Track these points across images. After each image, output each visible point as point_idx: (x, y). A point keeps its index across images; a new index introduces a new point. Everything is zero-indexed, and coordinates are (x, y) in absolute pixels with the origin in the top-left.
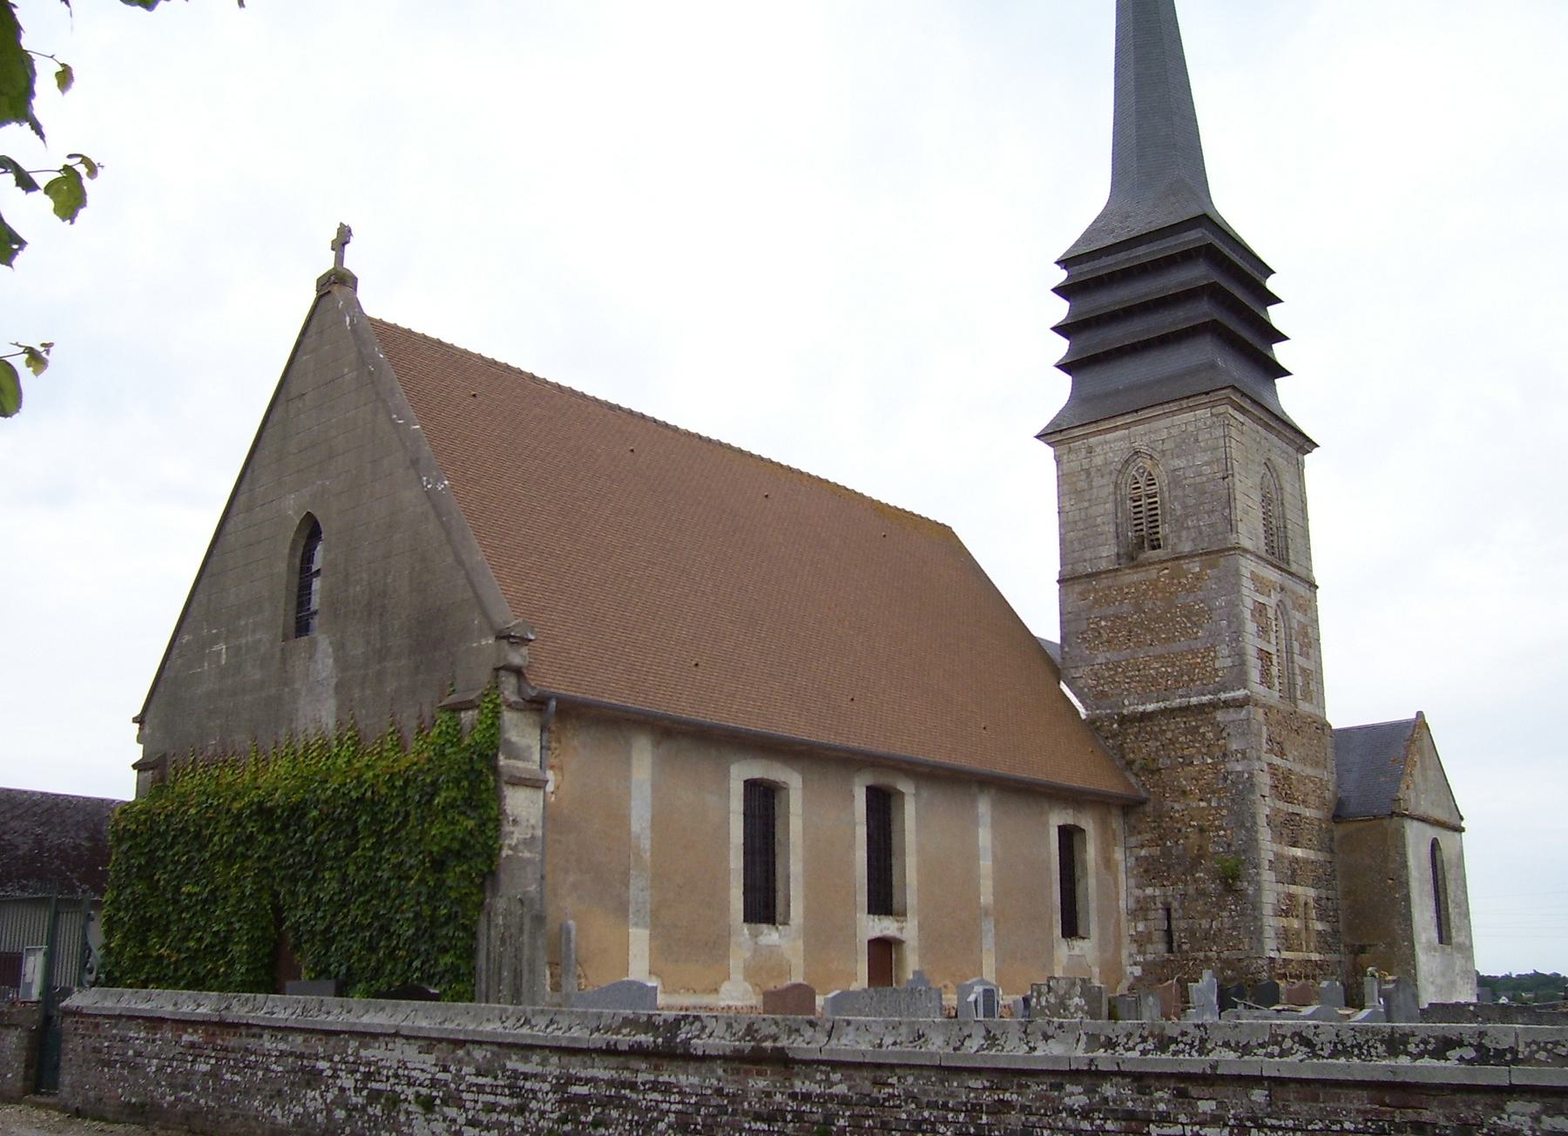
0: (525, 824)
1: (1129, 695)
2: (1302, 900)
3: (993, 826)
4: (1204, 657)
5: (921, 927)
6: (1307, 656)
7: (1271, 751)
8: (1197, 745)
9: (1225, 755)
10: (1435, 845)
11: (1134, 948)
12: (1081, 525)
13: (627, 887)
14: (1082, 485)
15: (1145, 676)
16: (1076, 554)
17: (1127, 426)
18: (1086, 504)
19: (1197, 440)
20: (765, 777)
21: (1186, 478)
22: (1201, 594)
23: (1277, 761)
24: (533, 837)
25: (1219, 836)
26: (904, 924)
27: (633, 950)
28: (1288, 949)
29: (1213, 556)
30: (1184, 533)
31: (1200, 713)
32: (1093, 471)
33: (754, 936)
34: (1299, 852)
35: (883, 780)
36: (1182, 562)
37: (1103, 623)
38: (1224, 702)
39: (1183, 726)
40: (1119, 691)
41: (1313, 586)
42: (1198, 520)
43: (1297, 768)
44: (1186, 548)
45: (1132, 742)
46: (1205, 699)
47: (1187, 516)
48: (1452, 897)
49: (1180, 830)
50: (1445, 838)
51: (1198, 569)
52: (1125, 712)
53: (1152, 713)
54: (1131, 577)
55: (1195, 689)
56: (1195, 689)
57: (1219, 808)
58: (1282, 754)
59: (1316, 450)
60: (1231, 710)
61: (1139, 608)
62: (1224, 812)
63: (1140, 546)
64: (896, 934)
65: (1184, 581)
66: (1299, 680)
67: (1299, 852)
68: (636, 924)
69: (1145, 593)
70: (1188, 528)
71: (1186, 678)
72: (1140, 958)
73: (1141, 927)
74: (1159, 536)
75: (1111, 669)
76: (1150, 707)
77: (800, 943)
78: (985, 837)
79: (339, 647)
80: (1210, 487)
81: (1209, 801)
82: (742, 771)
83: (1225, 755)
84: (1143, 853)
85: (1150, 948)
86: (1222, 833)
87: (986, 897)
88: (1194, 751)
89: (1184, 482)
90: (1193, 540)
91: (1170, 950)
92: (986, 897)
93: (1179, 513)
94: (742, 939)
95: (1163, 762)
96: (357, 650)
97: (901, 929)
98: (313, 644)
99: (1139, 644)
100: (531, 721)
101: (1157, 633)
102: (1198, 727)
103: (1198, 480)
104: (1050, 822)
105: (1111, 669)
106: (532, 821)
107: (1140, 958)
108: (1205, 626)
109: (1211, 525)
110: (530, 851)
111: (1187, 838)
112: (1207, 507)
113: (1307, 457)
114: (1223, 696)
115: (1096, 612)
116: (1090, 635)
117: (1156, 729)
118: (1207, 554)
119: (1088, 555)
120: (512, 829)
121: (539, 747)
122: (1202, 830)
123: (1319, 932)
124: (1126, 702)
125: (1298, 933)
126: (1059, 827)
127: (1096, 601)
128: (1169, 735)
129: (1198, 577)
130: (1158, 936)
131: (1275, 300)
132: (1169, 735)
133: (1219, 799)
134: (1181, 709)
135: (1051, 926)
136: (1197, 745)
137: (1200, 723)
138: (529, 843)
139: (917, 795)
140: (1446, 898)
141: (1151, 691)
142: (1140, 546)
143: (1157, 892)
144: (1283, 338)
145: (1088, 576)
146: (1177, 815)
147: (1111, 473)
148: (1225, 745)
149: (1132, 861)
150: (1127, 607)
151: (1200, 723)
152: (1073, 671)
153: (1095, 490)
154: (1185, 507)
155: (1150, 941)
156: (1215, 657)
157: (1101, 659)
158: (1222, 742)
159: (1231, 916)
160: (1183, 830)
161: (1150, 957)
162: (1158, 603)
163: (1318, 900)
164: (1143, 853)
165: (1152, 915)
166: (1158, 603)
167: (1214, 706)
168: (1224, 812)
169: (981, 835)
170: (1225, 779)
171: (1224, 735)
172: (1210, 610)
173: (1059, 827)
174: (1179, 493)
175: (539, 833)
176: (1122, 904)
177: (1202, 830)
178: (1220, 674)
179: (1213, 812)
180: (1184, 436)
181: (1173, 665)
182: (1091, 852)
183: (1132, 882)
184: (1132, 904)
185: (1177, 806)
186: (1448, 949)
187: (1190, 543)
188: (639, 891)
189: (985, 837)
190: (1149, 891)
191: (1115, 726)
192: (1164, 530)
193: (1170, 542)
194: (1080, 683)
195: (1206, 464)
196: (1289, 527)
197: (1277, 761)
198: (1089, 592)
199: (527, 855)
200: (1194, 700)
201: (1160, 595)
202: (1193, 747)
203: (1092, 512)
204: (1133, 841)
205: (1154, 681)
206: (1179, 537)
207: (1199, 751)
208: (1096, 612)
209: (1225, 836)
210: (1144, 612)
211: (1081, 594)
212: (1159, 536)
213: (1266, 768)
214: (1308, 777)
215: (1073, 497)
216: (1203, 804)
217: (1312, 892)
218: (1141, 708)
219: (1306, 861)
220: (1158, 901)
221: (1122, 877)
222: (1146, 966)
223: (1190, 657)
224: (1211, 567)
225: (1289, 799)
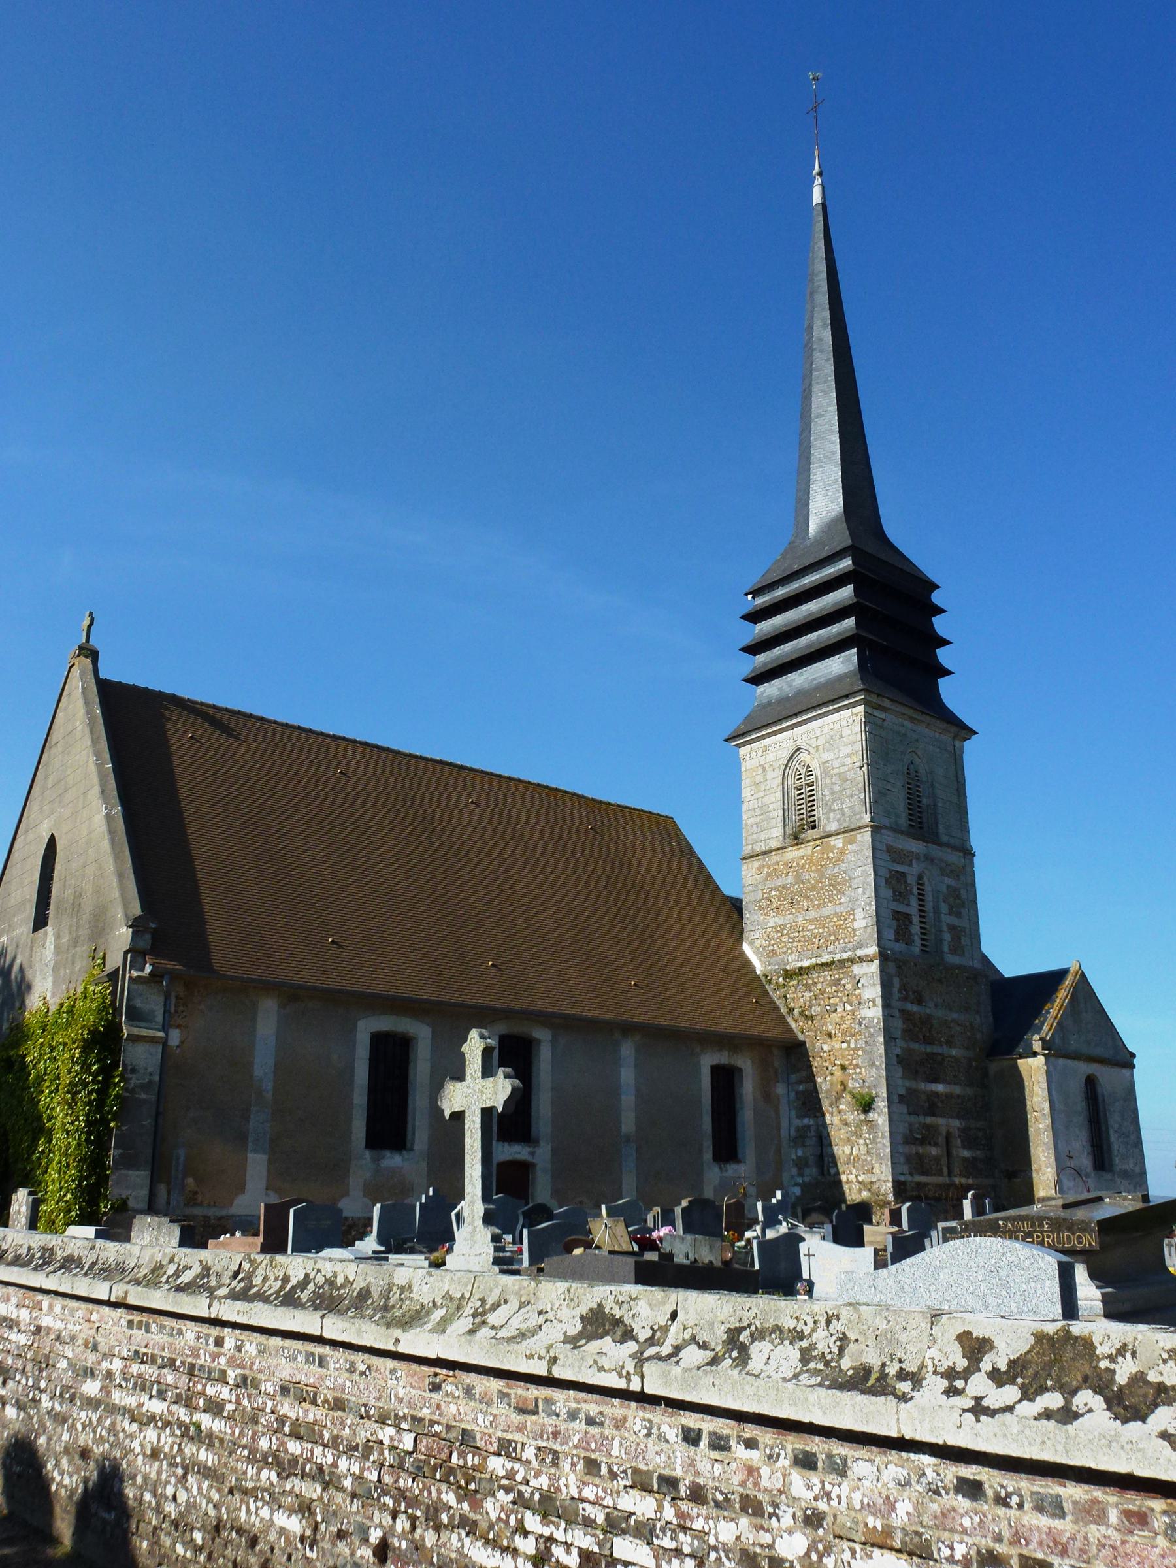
0: (142, 1071)
1: (792, 952)
2: (943, 1130)
3: (636, 1066)
4: (846, 919)
5: (554, 1151)
6: (959, 915)
7: (905, 999)
8: (840, 995)
9: (860, 1003)
10: (1091, 1082)
11: (794, 1171)
12: (758, 812)
13: (248, 1119)
14: (759, 778)
15: (803, 936)
16: (755, 836)
17: (792, 727)
18: (762, 794)
19: (841, 737)
20: (393, 1029)
21: (833, 769)
22: (843, 867)
23: (913, 1008)
24: (150, 1082)
25: (856, 1073)
26: (536, 1149)
27: (250, 1171)
28: (923, 1173)
29: (852, 833)
30: (832, 815)
31: (842, 968)
32: (767, 766)
33: (376, 1160)
34: (940, 1088)
35: (518, 1029)
36: (830, 839)
37: (773, 893)
38: (859, 958)
39: (829, 978)
40: (785, 950)
41: (969, 854)
42: (842, 803)
43: (940, 1013)
44: (833, 827)
45: (794, 993)
46: (845, 956)
47: (834, 800)
48: (1116, 1126)
49: (827, 1068)
50: (1107, 1076)
51: (841, 845)
52: (788, 968)
53: (808, 968)
54: (792, 853)
55: (839, 947)
56: (839, 947)
57: (856, 1049)
58: (919, 1001)
59: (974, 737)
60: (864, 964)
61: (798, 879)
62: (860, 1053)
63: (801, 829)
64: (529, 1159)
65: (831, 855)
66: (947, 937)
67: (940, 1088)
68: (255, 1151)
69: (803, 867)
70: (834, 811)
71: (832, 938)
72: (799, 1180)
73: (800, 1153)
74: (815, 818)
75: (778, 931)
76: (806, 963)
77: (424, 1165)
78: (627, 1076)
79: (58, 936)
80: (850, 775)
81: (848, 1043)
82: (367, 1027)
83: (860, 1003)
84: (801, 1088)
85: (807, 1171)
86: (858, 1070)
87: (628, 1123)
88: (838, 999)
89: (832, 772)
90: (838, 820)
91: (822, 1174)
92: (628, 1123)
93: (828, 798)
94: (364, 1162)
95: (816, 1010)
96: (65, 940)
97: (533, 1154)
98: (46, 934)
99: (798, 910)
100: (155, 990)
101: (812, 900)
102: (840, 980)
103: (842, 769)
104: (702, 1062)
105: (778, 931)
106: (150, 1070)
107: (799, 1180)
108: (846, 893)
109: (851, 807)
110: (146, 1093)
111: (832, 1074)
112: (848, 792)
113: (966, 743)
114: (860, 953)
115: (769, 884)
116: (764, 903)
117: (810, 981)
118: (847, 832)
119: (763, 836)
120: (130, 1076)
121: (162, 1011)
122: (843, 1068)
123: (965, 1160)
124: (790, 960)
125: (937, 1159)
126: (713, 1067)
127: (769, 875)
128: (819, 986)
129: (842, 852)
130: (812, 1160)
131: (940, 611)
132: (819, 986)
133: (856, 1041)
134: (827, 964)
135: (700, 1151)
136: (840, 995)
137: (842, 976)
138: (146, 1087)
139: (554, 1042)
140: (1107, 1129)
141: (808, 950)
142: (801, 829)
143: (812, 1123)
144: (946, 642)
145: (763, 854)
146: (825, 1055)
147: (779, 767)
148: (860, 995)
149: (793, 1095)
150: (790, 879)
151: (842, 976)
152: (752, 933)
153: (768, 782)
154: (832, 793)
155: (807, 1165)
156: (854, 919)
157: (772, 924)
158: (857, 992)
159: (866, 1144)
160: (830, 1068)
161: (807, 1179)
162: (813, 875)
163: (964, 1131)
164: (801, 1088)
165: (808, 1142)
166: (813, 875)
167: (851, 960)
168: (860, 1053)
169: (622, 1073)
170: (860, 1023)
171: (860, 985)
172: (850, 879)
173: (713, 1067)
174: (828, 781)
175: (157, 1078)
176: (784, 1133)
177: (843, 1068)
178: (858, 933)
179: (852, 1052)
180: (832, 733)
181: (824, 927)
182: (748, 1088)
183: (793, 1113)
184: (793, 1133)
185: (826, 1047)
186: (1108, 1176)
187: (836, 823)
188: (259, 1122)
189: (627, 1076)
190: (806, 1121)
191: (781, 979)
192: (819, 813)
193: (822, 823)
194: (757, 943)
195: (849, 756)
196: (940, 804)
197: (913, 1008)
198: (764, 866)
199: (143, 1096)
200: (837, 957)
201: (814, 868)
202: (838, 997)
203: (767, 800)
204: (794, 1078)
205: (810, 941)
206: (828, 819)
207: (841, 1000)
208: (769, 884)
209: (860, 1073)
210: (803, 883)
211: (759, 869)
212: (815, 818)
213: (897, 1014)
214: (953, 1021)
215: (753, 788)
216: (845, 1045)
217: (956, 1123)
218: (799, 964)
219: (948, 1096)
220: (813, 1129)
221: (784, 1107)
222: (803, 1186)
223: (835, 919)
224: (852, 842)
225: (928, 1041)
